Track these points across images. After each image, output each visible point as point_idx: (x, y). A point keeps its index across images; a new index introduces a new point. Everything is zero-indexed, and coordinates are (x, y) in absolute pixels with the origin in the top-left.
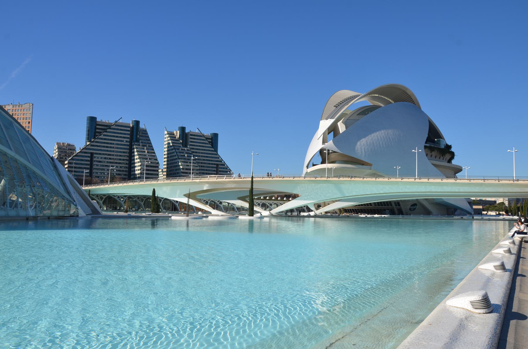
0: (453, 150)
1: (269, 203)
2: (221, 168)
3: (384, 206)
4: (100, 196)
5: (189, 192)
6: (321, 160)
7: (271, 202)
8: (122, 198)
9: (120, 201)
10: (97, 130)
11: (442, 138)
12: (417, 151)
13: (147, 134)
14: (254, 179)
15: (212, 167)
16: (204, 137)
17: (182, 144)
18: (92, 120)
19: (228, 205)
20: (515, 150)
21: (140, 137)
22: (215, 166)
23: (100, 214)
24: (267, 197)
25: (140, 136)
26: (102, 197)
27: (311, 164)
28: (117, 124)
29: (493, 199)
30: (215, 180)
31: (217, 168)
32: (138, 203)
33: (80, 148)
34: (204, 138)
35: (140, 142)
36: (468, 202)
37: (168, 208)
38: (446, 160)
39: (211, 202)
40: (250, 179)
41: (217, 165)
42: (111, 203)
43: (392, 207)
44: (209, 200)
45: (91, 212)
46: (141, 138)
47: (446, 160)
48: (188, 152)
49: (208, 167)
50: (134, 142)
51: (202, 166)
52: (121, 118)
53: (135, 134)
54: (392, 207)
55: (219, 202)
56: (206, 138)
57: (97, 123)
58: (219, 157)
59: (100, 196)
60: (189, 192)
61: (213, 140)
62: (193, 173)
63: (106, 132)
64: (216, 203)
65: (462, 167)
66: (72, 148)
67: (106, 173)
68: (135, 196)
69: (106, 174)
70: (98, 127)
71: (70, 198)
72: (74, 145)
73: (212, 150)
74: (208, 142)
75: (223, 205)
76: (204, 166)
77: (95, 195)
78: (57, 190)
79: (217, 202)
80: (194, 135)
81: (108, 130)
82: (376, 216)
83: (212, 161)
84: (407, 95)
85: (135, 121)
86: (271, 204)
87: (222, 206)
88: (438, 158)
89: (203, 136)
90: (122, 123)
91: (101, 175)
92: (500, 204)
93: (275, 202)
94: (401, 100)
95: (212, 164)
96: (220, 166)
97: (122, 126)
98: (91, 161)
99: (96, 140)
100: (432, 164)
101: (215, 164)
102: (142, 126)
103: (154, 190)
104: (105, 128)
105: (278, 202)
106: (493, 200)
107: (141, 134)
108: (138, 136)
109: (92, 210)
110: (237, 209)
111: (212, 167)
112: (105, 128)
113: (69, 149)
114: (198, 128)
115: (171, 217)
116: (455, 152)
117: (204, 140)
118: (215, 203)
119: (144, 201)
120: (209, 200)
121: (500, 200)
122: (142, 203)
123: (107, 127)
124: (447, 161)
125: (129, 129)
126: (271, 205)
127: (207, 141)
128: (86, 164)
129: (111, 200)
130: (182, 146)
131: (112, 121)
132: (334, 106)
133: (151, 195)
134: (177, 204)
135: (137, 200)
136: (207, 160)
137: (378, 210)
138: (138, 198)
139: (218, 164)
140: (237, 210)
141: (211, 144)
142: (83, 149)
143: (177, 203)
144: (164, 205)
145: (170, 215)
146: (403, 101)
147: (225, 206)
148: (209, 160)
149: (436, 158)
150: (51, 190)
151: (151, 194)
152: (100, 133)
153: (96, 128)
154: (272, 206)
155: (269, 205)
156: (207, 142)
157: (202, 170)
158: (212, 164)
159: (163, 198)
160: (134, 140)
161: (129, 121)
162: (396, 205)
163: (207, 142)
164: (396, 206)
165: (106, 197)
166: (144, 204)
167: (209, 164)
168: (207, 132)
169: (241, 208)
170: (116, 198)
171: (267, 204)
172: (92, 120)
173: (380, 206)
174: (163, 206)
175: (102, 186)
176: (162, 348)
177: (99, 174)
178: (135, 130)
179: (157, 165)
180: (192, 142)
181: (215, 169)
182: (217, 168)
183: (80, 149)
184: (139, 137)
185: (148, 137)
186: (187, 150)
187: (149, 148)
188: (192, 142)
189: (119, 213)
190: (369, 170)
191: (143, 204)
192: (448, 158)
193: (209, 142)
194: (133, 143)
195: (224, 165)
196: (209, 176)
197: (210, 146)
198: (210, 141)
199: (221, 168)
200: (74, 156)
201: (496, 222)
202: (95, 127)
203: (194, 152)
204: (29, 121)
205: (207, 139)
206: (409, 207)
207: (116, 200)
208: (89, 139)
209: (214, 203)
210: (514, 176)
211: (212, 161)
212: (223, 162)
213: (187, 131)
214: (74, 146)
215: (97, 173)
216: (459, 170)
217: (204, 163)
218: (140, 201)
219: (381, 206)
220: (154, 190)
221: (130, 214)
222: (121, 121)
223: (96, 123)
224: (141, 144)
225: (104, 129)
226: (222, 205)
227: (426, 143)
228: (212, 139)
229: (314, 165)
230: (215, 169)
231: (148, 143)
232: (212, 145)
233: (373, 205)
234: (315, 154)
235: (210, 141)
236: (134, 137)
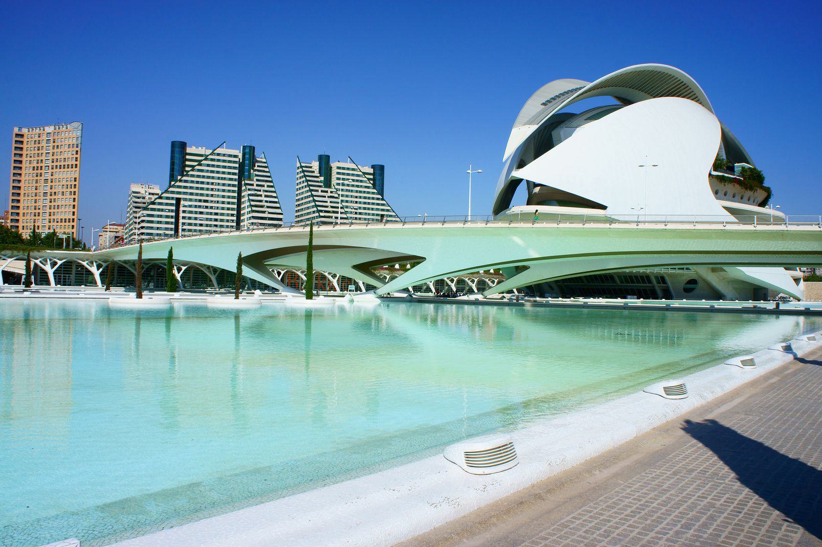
3: (643, 283)
11: (750, 162)
34: (361, 173)
41: (382, 216)
43: (651, 285)
47: (754, 202)
54: (651, 285)
56: (363, 173)
74: (367, 178)
77: (205, 265)
89: (358, 170)
99: (184, 178)
101: (377, 215)
108: (252, 171)
128: (170, 211)
129: (198, 273)
141: (372, 182)
146: (682, 95)
149: (734, 197)
151: (166, 256)
152: (193, 166)
162: (659, 283)
163: (366, 179)
164: (660, 283)
165: (149, 265)
173: (635, 283)
175: (671, 289)
176: (479, 540)
186: (331, 192)
193: (369, 179)
197: (370, 185)
198: (371, 177)
204: (77, 149)
206: (682, 285)
210: (469, 214)
219: (637, 283)
235: (371, 177)
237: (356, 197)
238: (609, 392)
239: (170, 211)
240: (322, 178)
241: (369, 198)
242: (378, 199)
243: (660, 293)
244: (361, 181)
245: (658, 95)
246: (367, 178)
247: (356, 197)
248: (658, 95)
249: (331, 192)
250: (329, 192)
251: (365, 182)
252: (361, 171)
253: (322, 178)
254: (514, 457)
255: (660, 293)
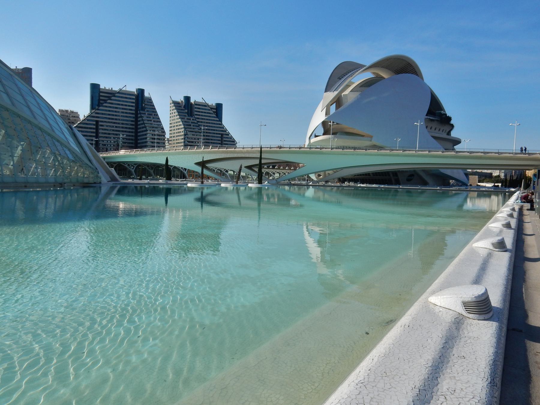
0: (452, 122)
1: (272, 172)
2: (226, 138)
4: (110, 164)
5: (203, 160)
6: (323, 132)
7: (274, 171)
8: (132, 166)
9: (130, 169)
10: (101, 98)
12: (419, 124)
13: (152, 102)
14: (262, 149)
15: (217, 137)
16: (209, 107)
17: (188, 113)
18: (95, 88)
19: (234, 173)
20: (517, 124)
21: (145, 106)
22: (220, 136)
23: (118, 180)
24: (270, 166)
25: (145, 105)
26: (113, 165)
27: (313, 135)
28: (120, 92)
29: (489, 171)
30: (129, 154)
31: (222, 137)
32: (148, 170)
33: (84, 116)
35: (146, 110)
36: (464, 173)
37: (176, 176)
38: (445, 132)
39: (218, 171)
40: (260, 149)
41: (222, 135)
42: (121, 171)
44: (216, 169)
45: (110, 180)
46: (146, 106)
47: (445, 132)
48: (193, 121)
49: (213, 137)
50: (139, 111)
51: (207, 136)
52: (126, 86)
53: (140, 102)
55: (225, 171)
56: (210, 108)
57: (101, 91)
58: (223, 127)
59: (110, 164)
60: (203, 160)
61: (218, 109)
62: (157, 146)
63: (111, 100)
64: (223, 171)
65: (461, 140)
66: (76, 115)
67: (112, 142)
68: (145, 164)
69: (112, 143)
70: (101, 94)
71: (91, 164)
72: (78, 113)
73: (216, 120)
74: (213, 112)
75: (229, 174)
76: (209, 136)
78: (81, 158)
79: (223, 170)
80: (199, 105)
81: (113, 98)
82: (374, 186)
83: (217, 130)
84: (411, 66)
85: (139, 89)
86: (274, 173)
87: (228, 174)
88: (437, 130)
90: (126, 91)
91: (107, 143)
92: (496, 177)
93: (278, 171)
94: (407, 71)
95: (217, 134)
96: (224, 136)
97: (125, 94)
98: (97, 129)
100: (432, 136)
101: (219, 134)
102: (146, 94)
103: (167, 158)
104: (109, 95)
105: (281, 171)
106: (490, 172)
107: (146, 103)
108: (144, 105)
109: (110, 178)
110: (230, 177)
111: (217, 137)
112: (109, 95)
113: (72, 116)
114: (202, 98)
115: (187, 184)
116: (455, 127)
117: (209, 110)
118: (221, 171)
119: (154, 169)
120: (216, 169)
121: (496, 173)
122: (133, 171)
123: (111, 94)
124: (446, 134)
125: (134, 97)
126: (274, 174)
127: (212, 111)
128: (92, 132)
130: (187, 116)
131: (116, 88)
132: (338, 78)
133: (165, 164)
134: (186, 173)
135: (147, 168)
136: (212, 130)
137: (352, 179)
138: (129, 165)
139: (223, 134)
140: (242, 178)
142: (87, 117)
143: (186, 171)
144: (173, 173)
145: (185, 182)
147: (231, 174)
148: (214, 130)
150: (75, 158)
151: (164, 162)
153: (100, 96)
154: (274, 175)
155: (272, 174)
156: (212, 112)
157: (207, 139)
158: (217, 134)
159: (172, 166)
160: (140, 108)
161: (132, 88)
163: (212, 112)
166: (154, 172)
167: (214, 133)
168: (212, 101)
169: (246, 177)
170: (126, 166)
171: (271, 173)
172: (95, 88)
174: (156, 173)
177: (105, 142)
178: (140, 99)
179: (163, 134)
180: (196, 111)
181: (220, 139)
182: (222, 137)
183: (84, 117)
184: (145, 105)
185: (154, 106)
187: (155, 117)
188: (196, 111)
189: (134, 180)
190: (369, 141)
191: (134, 171)
192: (448, 131)
194: (139, 112)
195: (228, 135)
196: (135, 150)
197: (215, 116)
198: (215, 111)
199: (226, 138)
200: (79, 124)
201: (89, 181)
202: (99, 94)
203: (199, 122)
205: (211, 108)
207: (126, 168)
208: (92, 107)
209: (220, 171)
211: (217, 130)
212: (227, 131)
213: (192, 101)
214: (77, 113)
215: (103, 141)
216: (457, 142)
217: (209, 133)
218: (150, 169)
220: (167, 158)
221: (388, 186)
222: (124, 89)
223: (100, 90)
224: (147, 113)
225: (108, 96)
226: (228, 173)
227: (427, 115)
228: (216, 109)
229: (316, 136)
230: (220, 139)
231: (153, 112)
232: (217, 115)
233: (371, 175)
234: (317, 127)
235: (215, 111)
236: (140, 106)
237: (207, 123)
238: (5, 78)
239: (92, 132)
240: (186, 111)
241: (113, 115)
242: (217, 121)
243: (393, 181)
244: (210, 113)
245: (405, 72)
246: (213, 112)
247: (207, 123)
248: (405, 72)
249: (193, 120)
250: (191, 119)
251: (212, 114)
252: (209, 107)
253: (186, 111)
254: (487, 302)
255: (393, 181)
